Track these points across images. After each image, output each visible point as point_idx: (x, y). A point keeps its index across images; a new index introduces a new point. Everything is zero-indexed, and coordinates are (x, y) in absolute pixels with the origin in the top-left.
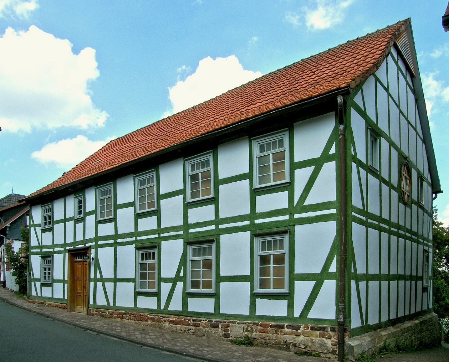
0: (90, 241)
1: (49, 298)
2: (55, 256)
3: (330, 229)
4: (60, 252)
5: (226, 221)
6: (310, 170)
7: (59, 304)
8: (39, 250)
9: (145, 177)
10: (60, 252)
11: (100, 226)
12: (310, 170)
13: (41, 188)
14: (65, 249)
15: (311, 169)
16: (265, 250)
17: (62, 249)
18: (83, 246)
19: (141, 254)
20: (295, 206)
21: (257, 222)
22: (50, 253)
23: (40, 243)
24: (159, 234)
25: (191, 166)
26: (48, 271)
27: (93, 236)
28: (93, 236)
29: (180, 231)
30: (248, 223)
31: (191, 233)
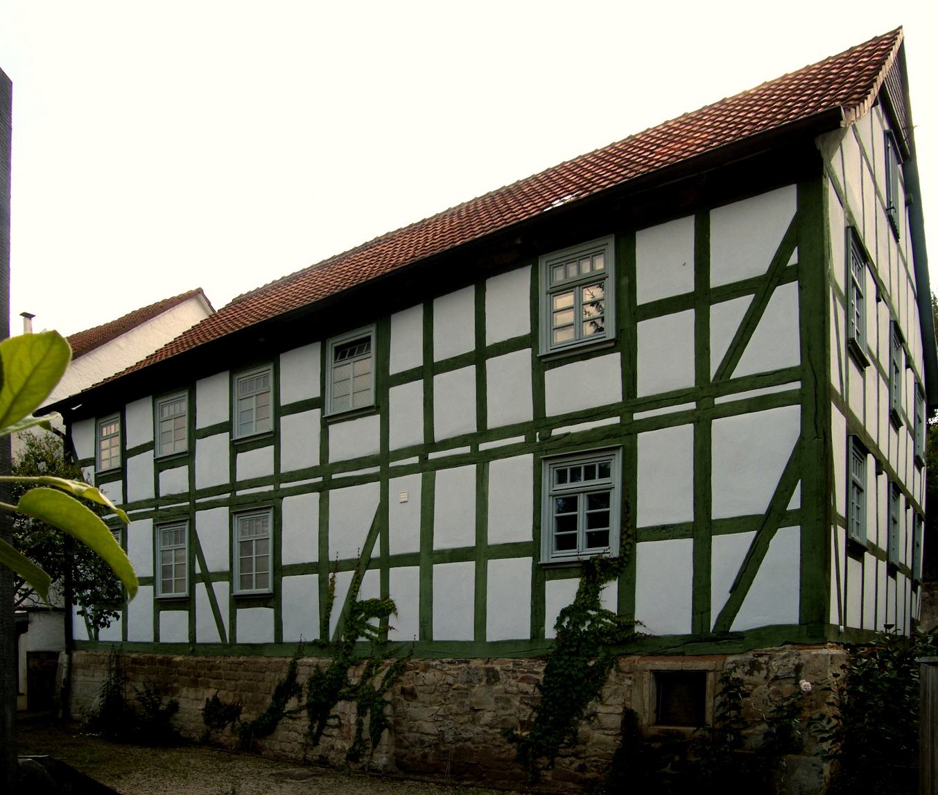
3: (785, 424)
5: (292, 476)
6: (743, 303)
12: (743, 303)
13: (173, 340)
15: (746, 301)
16: (566, 478)
19: (555, 472)
20: (711, 379)
21: (239, 493)
24: (157, 507)
27: (469, 425)
28: (469, 425)
30: (467, 450)
31: (721, 405)
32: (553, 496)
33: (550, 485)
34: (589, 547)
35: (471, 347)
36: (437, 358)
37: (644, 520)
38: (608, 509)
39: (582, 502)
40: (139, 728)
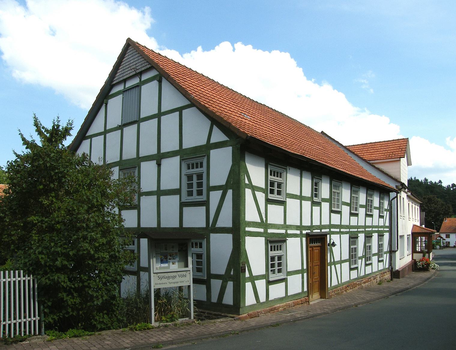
0: (325, 227)
1: (281, 299)
2: (290, 240)
4: (362, 232)
7: (302, 298)
8: (262, 230)
9: (190, 162)
10: (295, 236)
11: (185, 209)
14: (301, 232)
17: (298, 232)
18: (319, 231)
19: (187, 165)
22: (280, 236)
23: (264, 219)
25: (187, 166)
26: (275, 264)
29: (271, 233)
32: (186, 175)
33: (185, 171)
34: (188, 196)
35: (156, 112)
36: (162, 111)
37: (212, 184)
38: (202, 181)
39: (195, 177)
40: (232, 273)
